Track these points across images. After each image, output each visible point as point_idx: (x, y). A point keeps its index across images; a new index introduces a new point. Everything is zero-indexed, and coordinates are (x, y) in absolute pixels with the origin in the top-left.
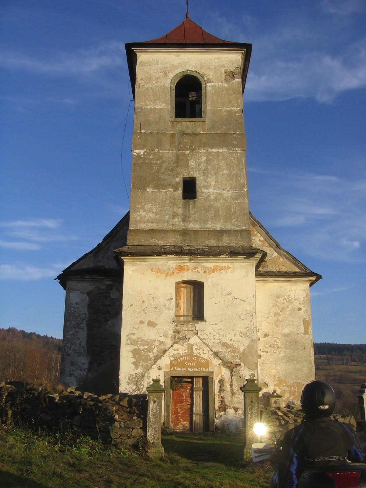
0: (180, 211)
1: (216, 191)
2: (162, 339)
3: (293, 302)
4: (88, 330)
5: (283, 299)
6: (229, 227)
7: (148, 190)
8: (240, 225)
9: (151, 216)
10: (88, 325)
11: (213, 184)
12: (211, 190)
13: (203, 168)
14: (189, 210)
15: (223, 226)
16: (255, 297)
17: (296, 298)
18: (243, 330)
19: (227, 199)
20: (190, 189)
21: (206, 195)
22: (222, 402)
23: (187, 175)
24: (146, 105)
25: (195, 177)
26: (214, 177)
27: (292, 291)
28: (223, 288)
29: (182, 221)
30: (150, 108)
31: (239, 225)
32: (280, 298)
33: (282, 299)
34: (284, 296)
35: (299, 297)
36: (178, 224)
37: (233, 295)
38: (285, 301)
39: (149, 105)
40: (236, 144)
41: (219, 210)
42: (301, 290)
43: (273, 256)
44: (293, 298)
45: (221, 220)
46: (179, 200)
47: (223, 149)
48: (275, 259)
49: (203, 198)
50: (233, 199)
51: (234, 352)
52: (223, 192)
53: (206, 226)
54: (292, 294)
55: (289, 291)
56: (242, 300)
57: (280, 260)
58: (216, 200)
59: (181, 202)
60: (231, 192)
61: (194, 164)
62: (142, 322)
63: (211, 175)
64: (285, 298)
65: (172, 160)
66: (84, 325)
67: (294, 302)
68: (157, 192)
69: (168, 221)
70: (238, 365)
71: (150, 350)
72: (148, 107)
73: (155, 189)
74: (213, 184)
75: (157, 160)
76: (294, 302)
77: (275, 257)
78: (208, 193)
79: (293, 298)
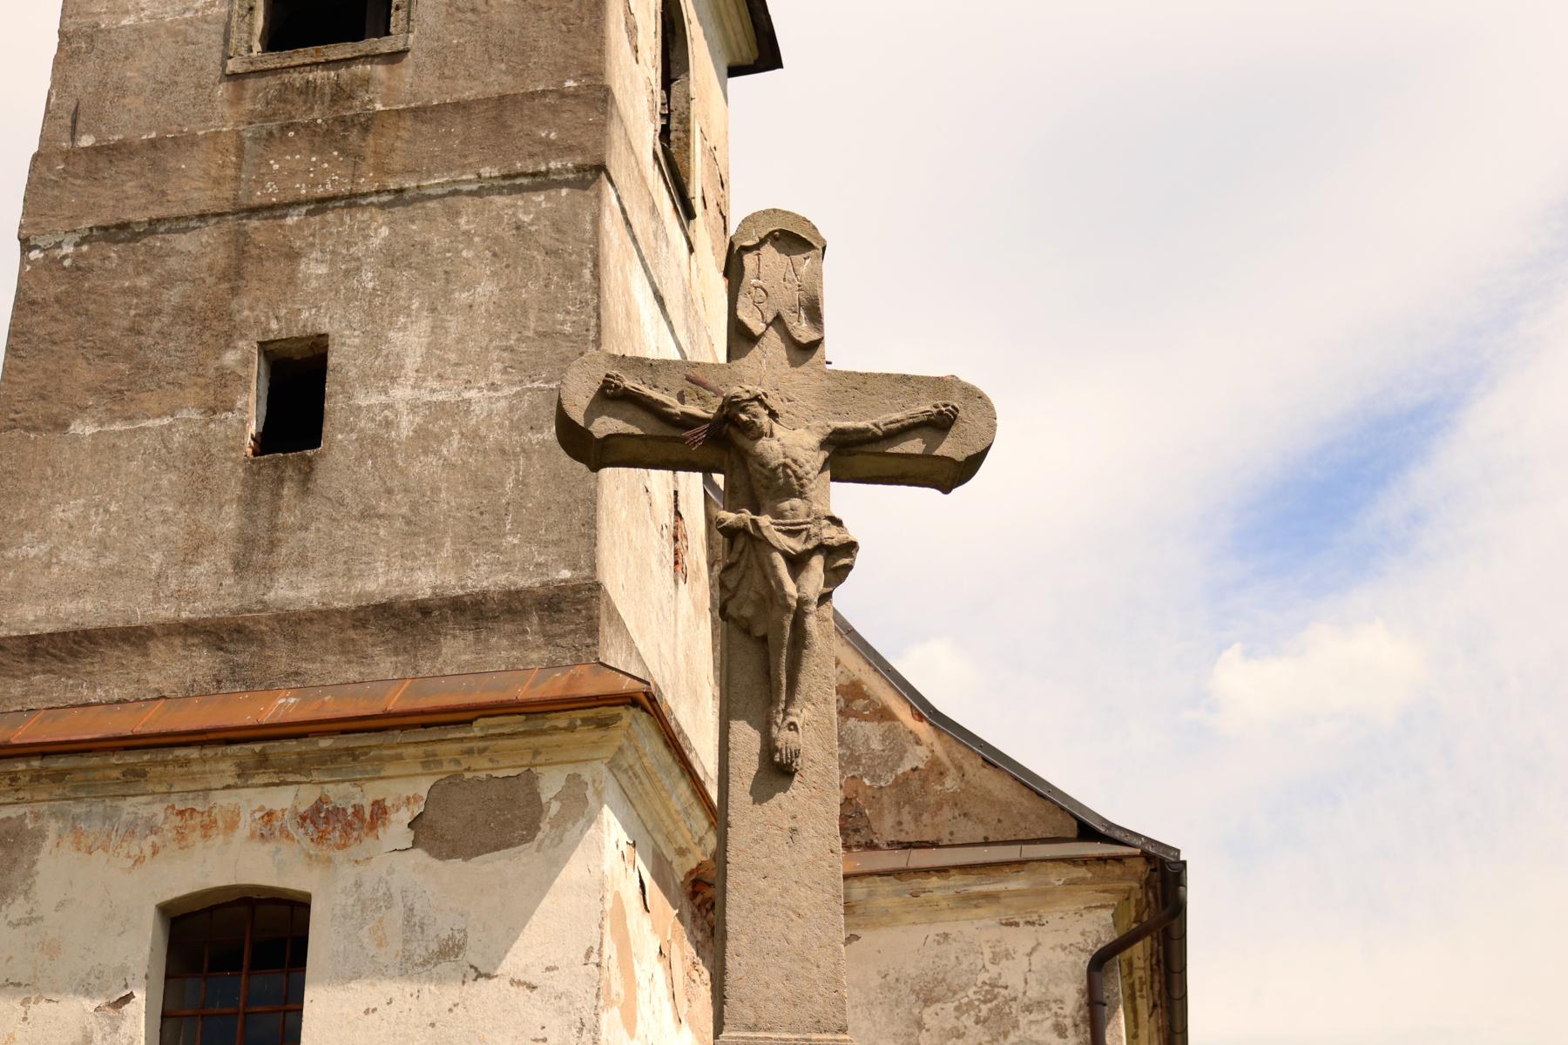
0: (229, 520)
1: (427, 397)
3: (1016, 1026)
5: (957, 1009)
6: (485, 577)
7: (76, 427)
8: (541, 559)
9: (80, 558)
11: (412, 362)
12: (401, 393)
13: (371, 285)
14: (275, 511)
15: (451, 579)
16: (594, 958)
17: (1034, 993)
19: (483, 431)
20: (297, 398)
21: (373, 420)
23: (280, 330)
25: (326, 336)
26: (425, 324)
27: (1007, 956)
28: (417, 919)
29: (230, 570)
30: (137, 30)
31: (538, 565)
32: (939, 1005)
33: (950, 1006)
34: (964, 988)
35: (1052, 988)
36: (212, 590)
37: (470, 956)
38: (968, 1020)
39: (127, 12)
40: (553, 143)
41: (436, 490)
42: (1064, 949)
43: (906, 766)
44: (1015, 999)
45: (439, 546)
46: (229, 464)
48: (915, 784)
49: (354, 436)
50: (514, 427)
52: (467, 395)
53: (358, 586)
54: (1012, 975)
55: (994, 961)
56: (520, 983)
57: (943, 784)
58: (424, 439)
59: (231, 474)
60: (506, 391)
61: (323, 270)
63: (409, 315)
64: (970, 1004)
65: (210, 268)
67: (1024, 1020)
68: (120, 434)
69: (159, 576)
72: (124, 22)
73: (113, 420)
74: (412, 362)
75: (139, 274)
76: (1024, 1020)
77: (915, 769)
78: (387, 407)
79: (1015, 999)
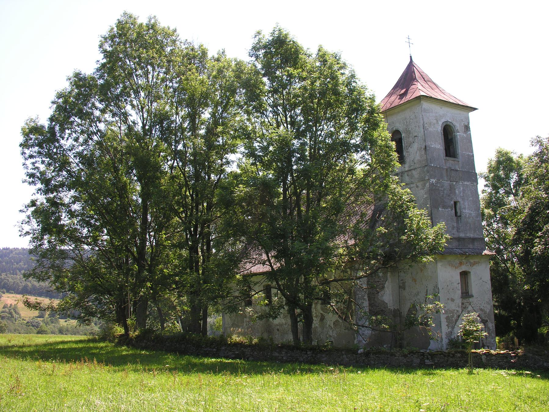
0: (455, 225)
2: (457, 309)
4: (369, 300)
10: (368, 297)
12: (467, 211)
18: (488, 300)
22: (483, 343)
24: (431, 145)
47: (73, 86)
51: (485, 314)
62: (448, 299)
66: (366, 297)
70: (487, 321)
71: (453, 316)
